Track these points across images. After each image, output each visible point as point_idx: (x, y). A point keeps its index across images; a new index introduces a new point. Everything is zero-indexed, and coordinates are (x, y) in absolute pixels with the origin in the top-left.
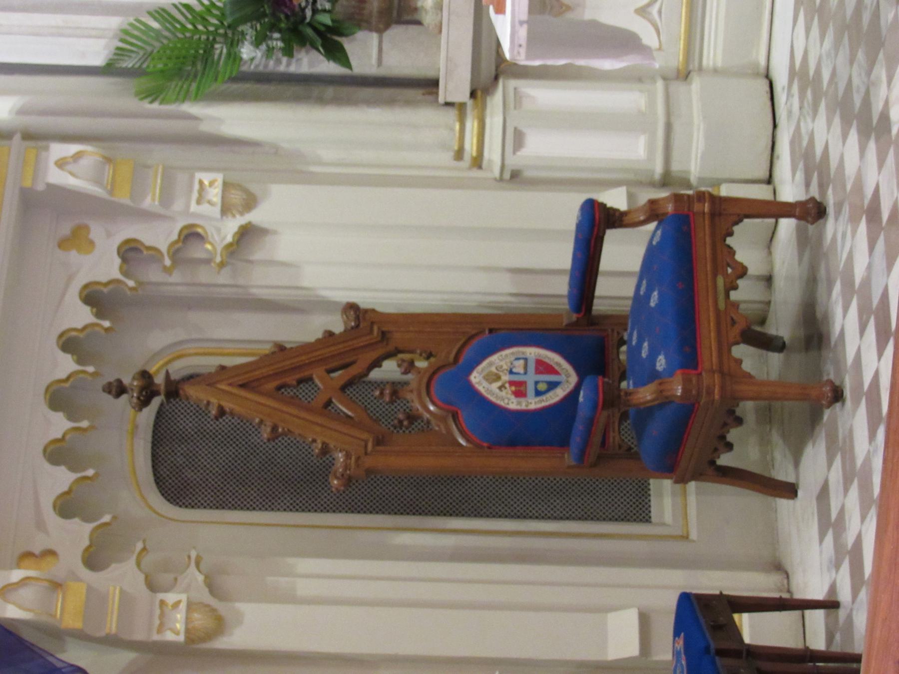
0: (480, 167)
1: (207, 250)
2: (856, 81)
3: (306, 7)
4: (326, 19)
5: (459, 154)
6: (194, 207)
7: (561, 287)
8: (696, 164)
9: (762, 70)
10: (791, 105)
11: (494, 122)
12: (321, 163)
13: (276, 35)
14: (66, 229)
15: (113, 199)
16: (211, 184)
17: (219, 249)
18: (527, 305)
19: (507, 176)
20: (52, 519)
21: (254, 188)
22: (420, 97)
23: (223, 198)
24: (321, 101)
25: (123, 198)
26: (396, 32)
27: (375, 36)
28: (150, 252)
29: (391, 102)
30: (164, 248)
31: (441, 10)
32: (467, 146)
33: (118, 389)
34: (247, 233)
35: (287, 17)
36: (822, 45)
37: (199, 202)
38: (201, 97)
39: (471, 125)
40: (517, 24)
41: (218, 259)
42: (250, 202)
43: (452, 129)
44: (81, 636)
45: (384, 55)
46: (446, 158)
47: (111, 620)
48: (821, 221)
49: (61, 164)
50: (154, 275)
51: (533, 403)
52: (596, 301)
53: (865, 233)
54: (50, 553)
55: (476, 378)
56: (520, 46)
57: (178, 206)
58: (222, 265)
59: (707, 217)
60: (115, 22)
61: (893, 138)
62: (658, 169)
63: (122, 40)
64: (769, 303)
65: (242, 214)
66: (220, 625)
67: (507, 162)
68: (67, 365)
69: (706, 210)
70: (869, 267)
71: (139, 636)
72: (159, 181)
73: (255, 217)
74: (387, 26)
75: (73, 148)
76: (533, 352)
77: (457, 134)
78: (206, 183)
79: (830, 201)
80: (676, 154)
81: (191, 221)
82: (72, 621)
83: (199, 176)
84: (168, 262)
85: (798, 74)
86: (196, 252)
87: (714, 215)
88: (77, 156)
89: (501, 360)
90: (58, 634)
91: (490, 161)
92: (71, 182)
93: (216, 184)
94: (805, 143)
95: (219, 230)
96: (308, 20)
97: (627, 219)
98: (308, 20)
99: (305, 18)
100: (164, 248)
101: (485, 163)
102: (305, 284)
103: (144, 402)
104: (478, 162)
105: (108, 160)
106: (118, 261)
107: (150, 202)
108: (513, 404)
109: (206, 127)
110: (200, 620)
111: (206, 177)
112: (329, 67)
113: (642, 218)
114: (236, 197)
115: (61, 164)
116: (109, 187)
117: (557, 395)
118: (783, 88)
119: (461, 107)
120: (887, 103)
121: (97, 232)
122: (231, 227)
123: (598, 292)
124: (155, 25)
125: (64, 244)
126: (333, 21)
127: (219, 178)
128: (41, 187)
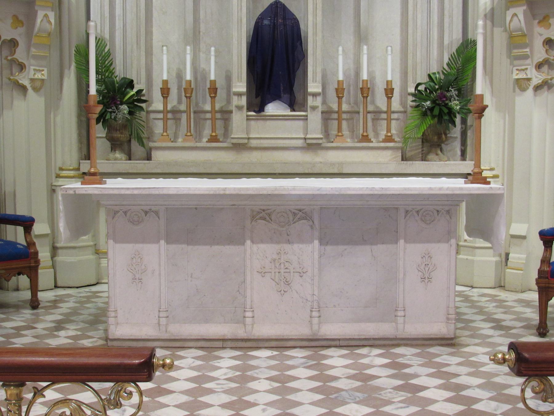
0: (56, 177)
1: (16, 73)
2: (81, 317)
3: (112, 109)
4: (108, 117)
5: (61, 169)
6: (32, 68)
7: (9, 211)
8: (65, 259)
9: (100, 281)
10: (83, 293)
12: (55, 116)
13: (101, 98)
14: (21, 18)
15: (33, 37)
16: (43, 74)
17: (16, 78)
19: (53, 188)
21: (42, 90)
22: (83, 153)
23: (36, 79)
25: (34, 40)
26: (108, 144)
27: (104, 135)
28: (13, 52)
29: (80, 142)
30: (15, 56)
31: (115, 160)
32: (64, 172)
34: (23, 89)
35: (108, 102)
36: (102, 303)
37: (34, 70)
39: (72, 173)
40: (74, 190)
41: (12, 78)
43: (70, 166)
45: (99, 139)
46: (59, 164)
48: (31, 308)
49: (46, 16)
52: (4, 225)
53: (21, 325)
56: (66, 191)
57: (32, 61)
58: (10, 79)
59: (29, 265)
61: (53, 333)
62: (58, 245)
63: (99, 39)
64: (8, 290)
65: (31, 86)
67: (58, 187)
69: (32, 265)
70: (6, 328)
72: (42, 54)
73: (30, 91)
74: (108, 140)
77: (68, 168)
78: (43, 73)
79: (39, 311)
80: (65, 251)
81: (27, 67)
83: (46, 70)
84: (9, 58)
85: (95, 295)
86: (15, 69)
87: (30, 268)
88: (50, 23)
91: (58, 181)
92: (39, 21)
93: (43, 76)
94: (66, 299)
95: (24, 77)
96: (107, 110)
97: (27, 234)
98: (107, 110)
99: (108, 109)
100: (15, 56)
101: (57, 179)
102: (4, 112)
104: (58, 176)
105: (49, 34)
106: (9, 38)
107: (33, 50)
109: (66, 71)
111: (45, 72)
113: (28, 240)
114: (38, 84)
115: (46, 16)
116: (38, 35)
118: (91, 290)
119: (78, 169)
120: (68, 329)
121: (21, 30)
123: (7, 225)
124: (106, 50)
126: (108, 119)
127: (45, 77)
128: (36, 8)
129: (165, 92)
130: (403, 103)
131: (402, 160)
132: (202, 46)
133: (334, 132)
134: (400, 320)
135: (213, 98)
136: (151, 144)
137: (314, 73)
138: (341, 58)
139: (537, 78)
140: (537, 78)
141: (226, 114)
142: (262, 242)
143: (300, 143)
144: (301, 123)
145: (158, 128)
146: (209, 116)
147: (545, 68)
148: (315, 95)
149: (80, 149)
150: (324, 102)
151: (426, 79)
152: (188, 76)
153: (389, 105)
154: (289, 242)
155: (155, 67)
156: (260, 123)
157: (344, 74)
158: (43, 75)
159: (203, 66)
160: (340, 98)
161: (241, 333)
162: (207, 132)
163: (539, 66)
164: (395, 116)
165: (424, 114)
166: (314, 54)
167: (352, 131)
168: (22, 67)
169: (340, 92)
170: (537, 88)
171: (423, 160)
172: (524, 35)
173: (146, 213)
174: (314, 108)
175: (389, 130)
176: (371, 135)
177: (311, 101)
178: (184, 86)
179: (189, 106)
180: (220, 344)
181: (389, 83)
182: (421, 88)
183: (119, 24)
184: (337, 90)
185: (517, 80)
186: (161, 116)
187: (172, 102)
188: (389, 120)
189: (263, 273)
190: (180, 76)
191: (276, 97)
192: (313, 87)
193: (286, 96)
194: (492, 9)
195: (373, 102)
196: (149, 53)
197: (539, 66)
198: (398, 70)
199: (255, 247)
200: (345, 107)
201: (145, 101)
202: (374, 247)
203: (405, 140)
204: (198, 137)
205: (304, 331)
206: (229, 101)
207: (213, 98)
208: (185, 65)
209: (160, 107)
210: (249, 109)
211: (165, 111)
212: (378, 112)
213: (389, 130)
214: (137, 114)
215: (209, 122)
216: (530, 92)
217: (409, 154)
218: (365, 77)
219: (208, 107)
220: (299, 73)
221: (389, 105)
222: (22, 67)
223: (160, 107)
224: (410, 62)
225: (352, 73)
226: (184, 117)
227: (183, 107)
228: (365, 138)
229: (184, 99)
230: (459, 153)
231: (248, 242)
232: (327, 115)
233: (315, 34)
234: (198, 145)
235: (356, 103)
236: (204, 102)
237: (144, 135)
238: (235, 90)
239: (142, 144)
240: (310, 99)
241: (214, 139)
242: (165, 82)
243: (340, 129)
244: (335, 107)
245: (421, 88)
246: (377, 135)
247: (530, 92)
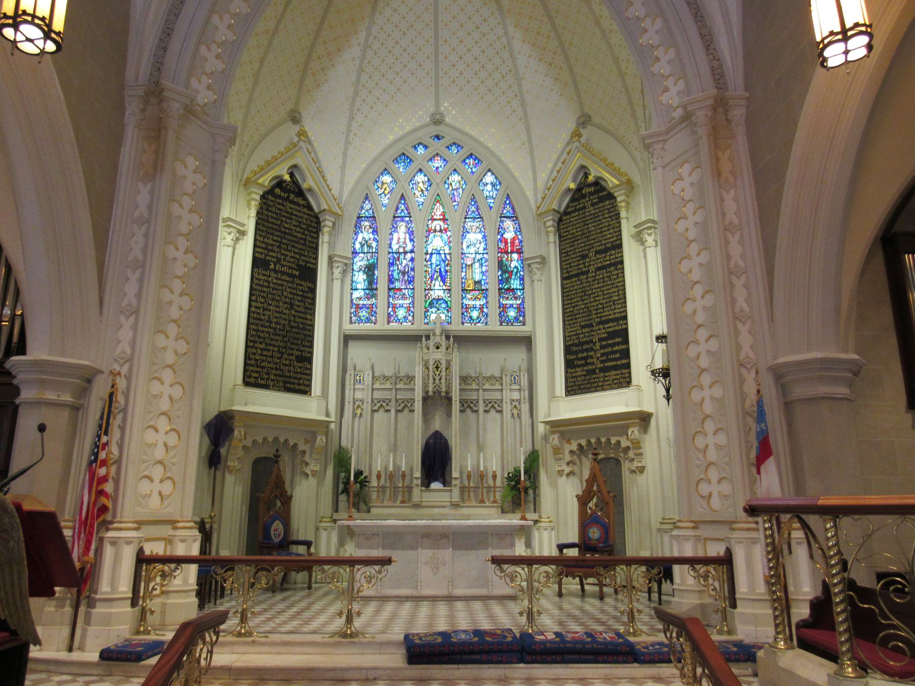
5: (322, 518)
7: (295, 538)
11: (329, 524)
14: (308, 439)
18: (291, 533)
20: (252, 439)
24: (333, 490)
25: (315, 451)
29: (333, 503)
33: (277, 451)
34: (307, 475)
38: (334, 465)
39: (328, 520)
42: (313, 476)
44: (229, 446)
46: (322, 515)
47: (894, 498)
50: (299, 457)
51: (272, 533)
54: (245, 439)
55: (278, 522)
60: (349, 447)
66: (230, 472)
68: (282, 440)
71: (229, 456)
73: (310, 477)
75: (324, 441)
76: (282, 533)
82: (233, 444)
86: (303, 465)
89: (281, 526)
90: (231, 440)
92: (318, 441)
103: (275, 456)
104: (321, 521)
108: (272, 529)
109: (328, 466)
110: (231, 468)
112: (340, 489)
115: (321, 439)
117: (273, 537)
121: (308, 446)
122: (308, 472)
125: (306, 439)
129: (379, 477)
130: (502, 483)
131: (502, 512)
132: (398, 453)
133: (466, 498)
134: (490, 587)
135: (403, 480)
136: (371, 505)
137: (455, 467)
138: (469, 460)
139: (567, 470)
140: (567, 470)
141: (410, 489)
142: (426, 549)
143: (448, 504)
144: (449, 493)
145: (374, 496)
146: (401, 489)
147: (571, 465)
148: (456, 479)
149: (333, 507)
150: (461, 482)
151: (513, 470)
152: (391, 469)
153: (495, 484)
154: (438, 549)
155: (374, 465)
156: (428, 493)
157: (471, 467)
158: (317, 468)
159: (399, 463)
160: (469, 480)
161: (415, 593)
162: (400, 498)
163: (568, 464)
164: (497, 489)
165: (512, 489)
166: (455, 458)
167: (476, 497)
168: (307, 464)
169: (469, 477)
170: (568, 475)
171: (513, 513)
172: (559, 449)
173: (373, 535)
174: (455, 486)
175: (495, 497)
176: (486, 500)
177: (454, 482)
178: (388, 473)
179: (391, 484)
180: (405, 599)
181: (494, 472)
182: (511, 475)
183: (355, 441)
184: (467, 476)
185: (558, 471)
186: (376, 489)
187: (382, 482)
188: (495, 492)
189: (426, 563)
190: (386, 468)
191: (436, 480)
192: (455, 474)
193: (441, 480)
194: (545, 435)
195: (487, 482)
196: (371, 456)
197: (568, 464)
198: (499, 464)
199: (423, 551)
200: (472, 485)
201: (368, 482)
202: (478, 551)
203: (503, 502)
204: (395, 501)
205: (445, 592)
206: (411, 482)
207: (403, 480)
208: (389, 462)
209: (376, 485)
210: (422, 486)
211: (378, 487)
212: (489, 487)
213: (495, 497)
214: (364, 489)
215: (401, 493)
216: (564, 477)
217: (506, 510)
218: (482, 469)
219: (400, 485)
220: (448, 468)
221: (495, 484)
222: (307, 464)
223: (376, 485)
224: (505, 462)
225: (476, 467)
226: (388, 489)
227: (388, 485)
228: (482, 501)
229: (388, 481)
230: (532, 509)
231: (420, 549)
232: (462, 489)
233: (456, 448)
234: (395, 505)
235: (478, 483)
236: (399, 482)
237: (367, 500)
238: (415, 476)
239: (366, 504)
240: (453, 480)
241: (403, 502)
242: (379, 472)
243: (469, 497)
244: (467, 485)
245: (511, 475)
246: (489, 499)
247: (564, 477)
